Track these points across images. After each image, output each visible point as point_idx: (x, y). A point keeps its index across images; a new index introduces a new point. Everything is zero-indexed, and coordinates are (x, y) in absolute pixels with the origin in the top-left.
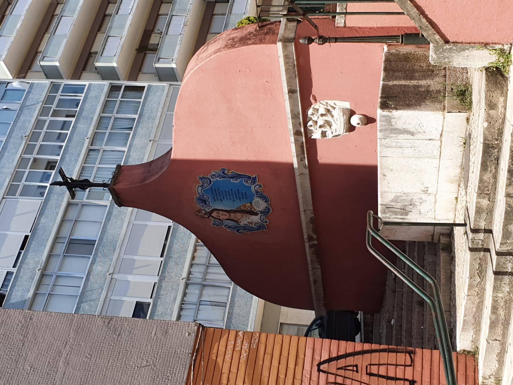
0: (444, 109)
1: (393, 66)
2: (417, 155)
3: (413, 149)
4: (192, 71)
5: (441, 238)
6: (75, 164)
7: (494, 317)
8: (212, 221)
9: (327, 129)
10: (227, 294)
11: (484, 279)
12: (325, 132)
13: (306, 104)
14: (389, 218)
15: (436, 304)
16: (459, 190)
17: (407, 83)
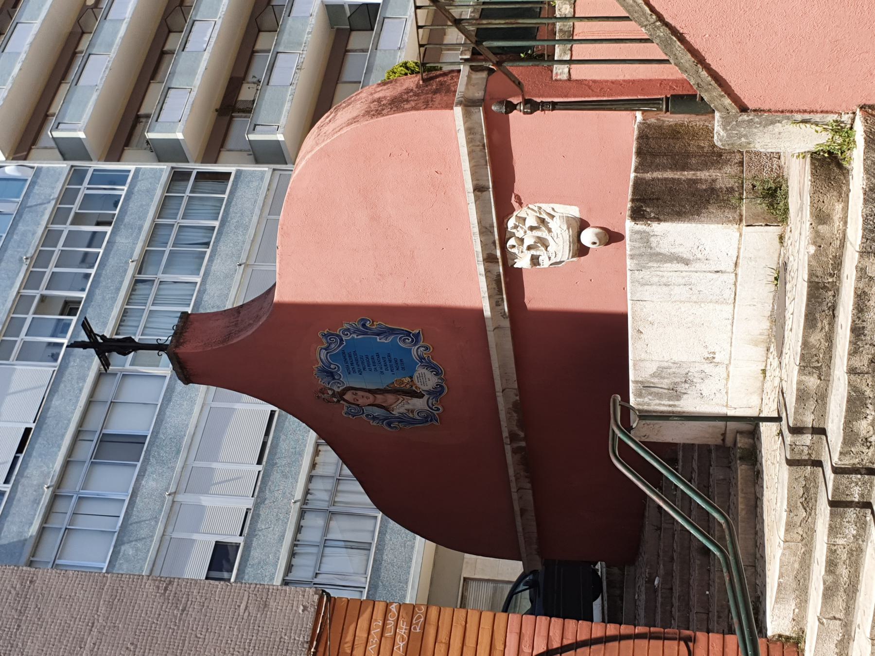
0: (741, 220)
1: (651, 148)
2: (694, 298)
3: (687, 288)
4: (309, 156)
5: (738, 438)
6: (112, 306)
7: (830, 579)
8: (345, 409)
9: (540, 252)
10: (372, 529)
11: (813, 514)
12: (538, 257)
13: (504, 211)
14: (649, 404)
15: (731, 558)
16: (767, 358)
17: (677, 175)
